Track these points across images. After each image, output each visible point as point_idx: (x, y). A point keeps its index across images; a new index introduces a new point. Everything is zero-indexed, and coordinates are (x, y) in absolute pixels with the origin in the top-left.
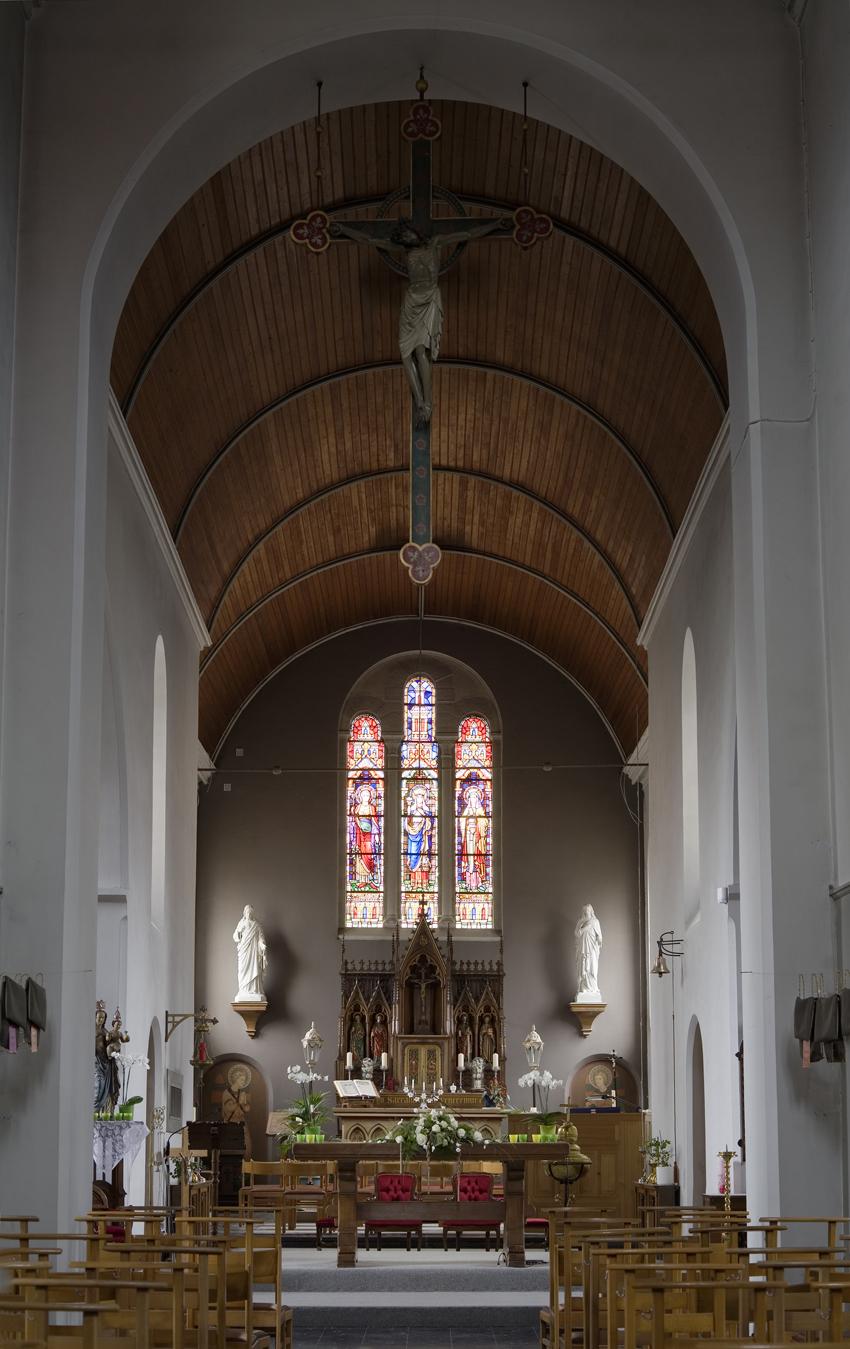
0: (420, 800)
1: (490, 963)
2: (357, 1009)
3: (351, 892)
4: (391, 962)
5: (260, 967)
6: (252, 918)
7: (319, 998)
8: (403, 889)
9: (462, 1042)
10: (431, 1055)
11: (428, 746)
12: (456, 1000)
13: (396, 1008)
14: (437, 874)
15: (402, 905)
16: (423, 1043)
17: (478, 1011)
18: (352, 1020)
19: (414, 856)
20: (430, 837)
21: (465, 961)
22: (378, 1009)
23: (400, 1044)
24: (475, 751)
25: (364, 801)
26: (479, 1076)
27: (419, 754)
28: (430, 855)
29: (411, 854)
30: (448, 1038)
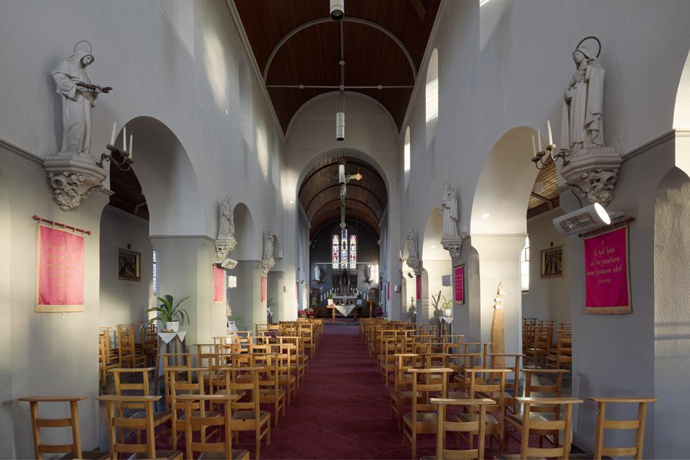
7: (329, 279)
24: (353, 240)
25: (335, 249)
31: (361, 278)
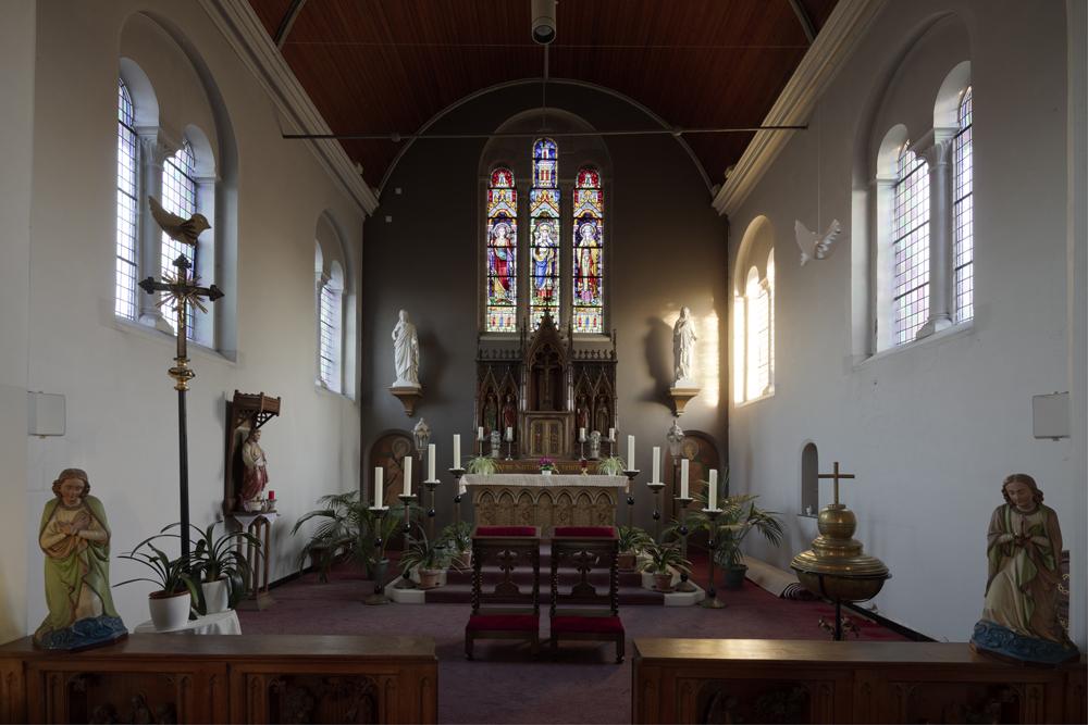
0: (545, 235)
1: (605, 353)
2: (490, 390)
4: (520, 351)
5: (413, 360)
6: (407, 320)
7: (462, 382)
8: (532, 303)
10: (554, 429)
11: (552, 193)
12: (575, 382)
13: (524, 390)
16: (547, 419)
17: (595, 392)
18: (487, 400)
20: (553, 264)
21: (583, 351)
22: (509, 391)
24: (588, 200)
25: (501, 235)
27: (545, 201)
28: (553, 277)
31: (632, 378)
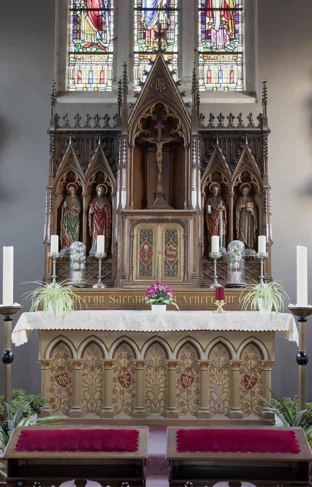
2: (70, 178)
3: (75, 53)
4: (116, 117)
9: (213, 221)
10: (170, 237)
12: (204, 164)
13: (124, 175)
14: (176, 33)
15: (135, 68)
19: (150, 12)
21: (216, 115)
22: (99, 178)
23: (127, 222)
26: (237, 265)
29: (146, 9)
30: (194, 213)
